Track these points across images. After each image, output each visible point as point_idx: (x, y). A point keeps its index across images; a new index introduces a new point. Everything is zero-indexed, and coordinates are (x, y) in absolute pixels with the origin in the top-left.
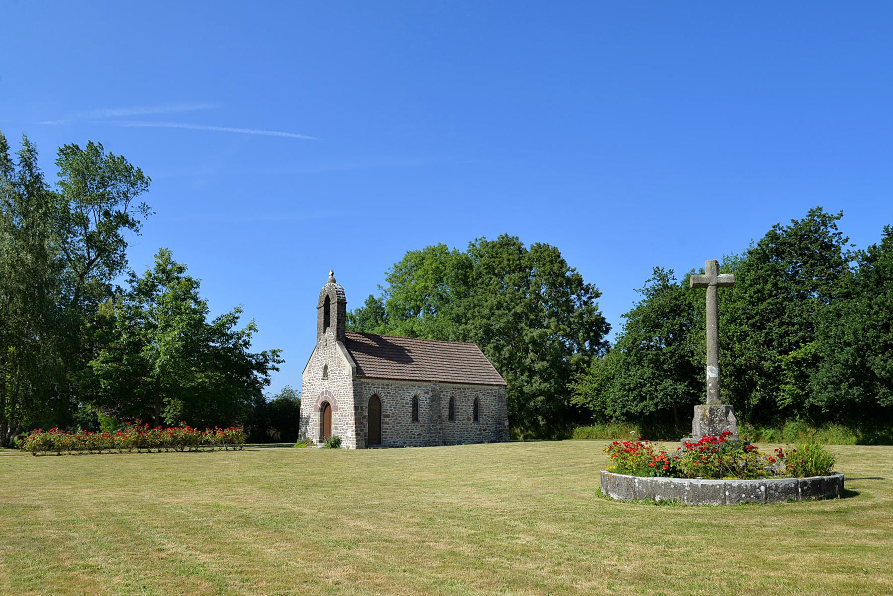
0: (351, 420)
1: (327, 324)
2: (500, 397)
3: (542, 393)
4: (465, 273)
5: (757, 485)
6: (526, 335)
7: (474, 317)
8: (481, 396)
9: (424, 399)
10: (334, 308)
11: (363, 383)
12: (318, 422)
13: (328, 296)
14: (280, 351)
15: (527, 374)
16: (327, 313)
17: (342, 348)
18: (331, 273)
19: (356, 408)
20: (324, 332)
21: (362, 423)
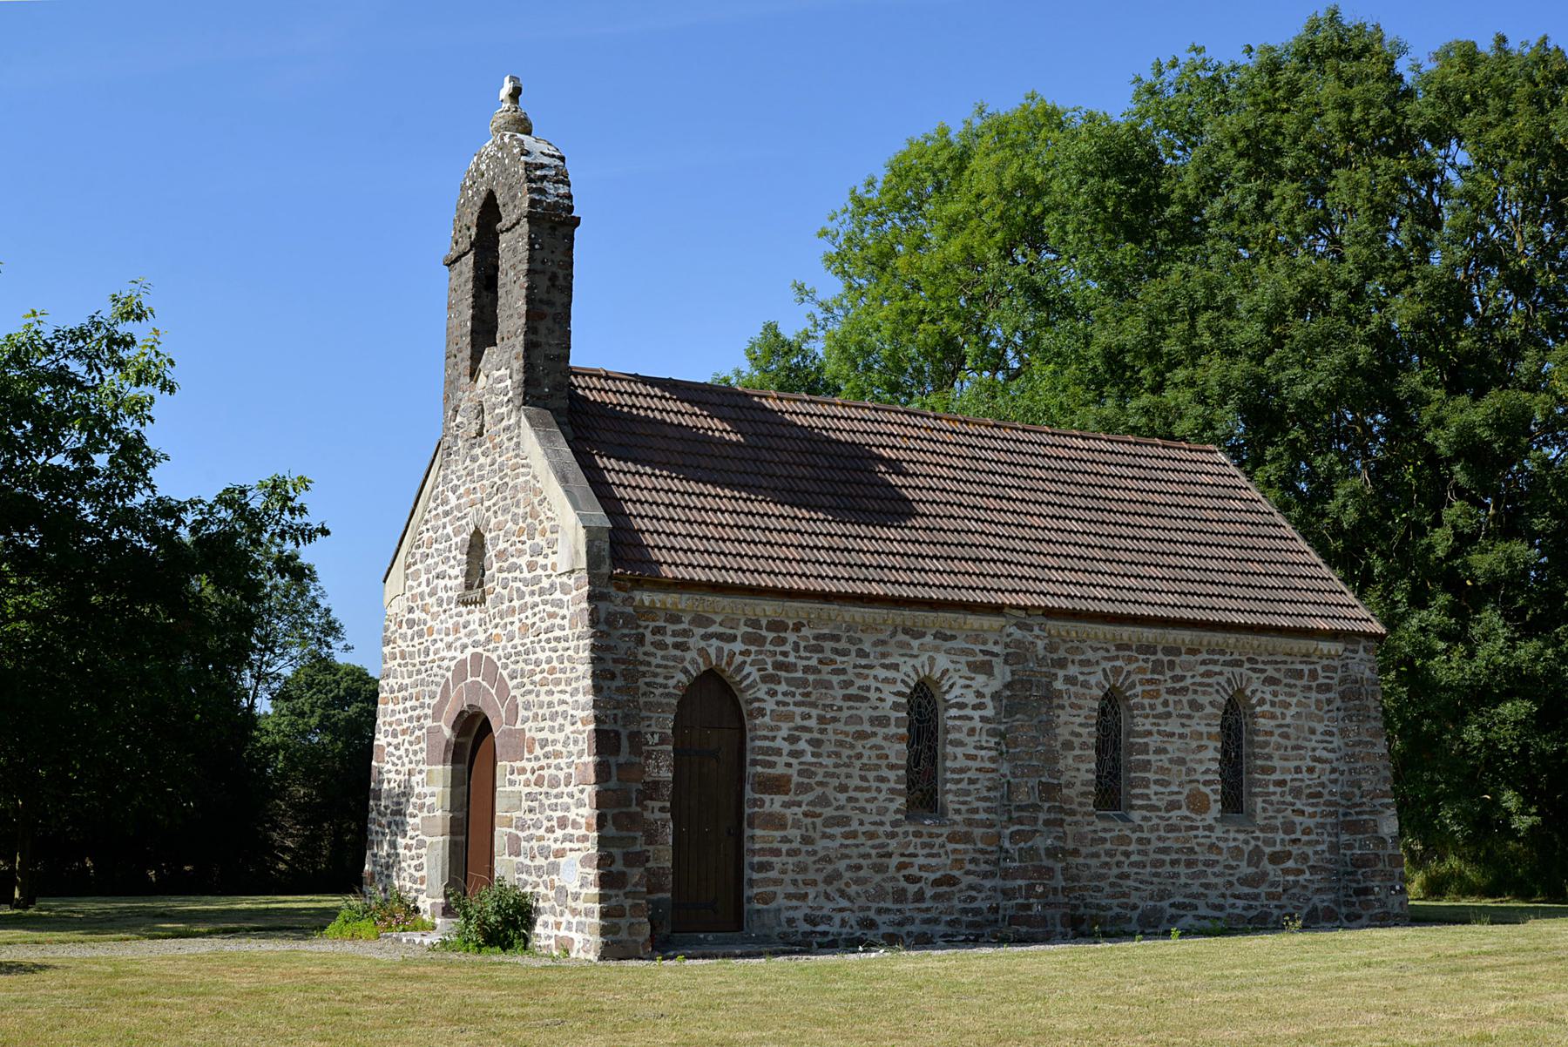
0: (579, 806)
1: (484, 332)
2: (1352, 692)
3: (1517, 683)
4: (1134, 194)
6: (1439, 422)
7: (1195, 353)
8: (1256, 687)
9: (969, 697)
10: (513, 248)
11: (650, 612)
12: (441, 815)
13: (491, 195)
14: (305, 483)
15: (1443, 599)
16: (486, 283)
17: (545, 439)
18: (507, 87)
19: (605, 741)
20: (473, 374)
21: (634, 820)
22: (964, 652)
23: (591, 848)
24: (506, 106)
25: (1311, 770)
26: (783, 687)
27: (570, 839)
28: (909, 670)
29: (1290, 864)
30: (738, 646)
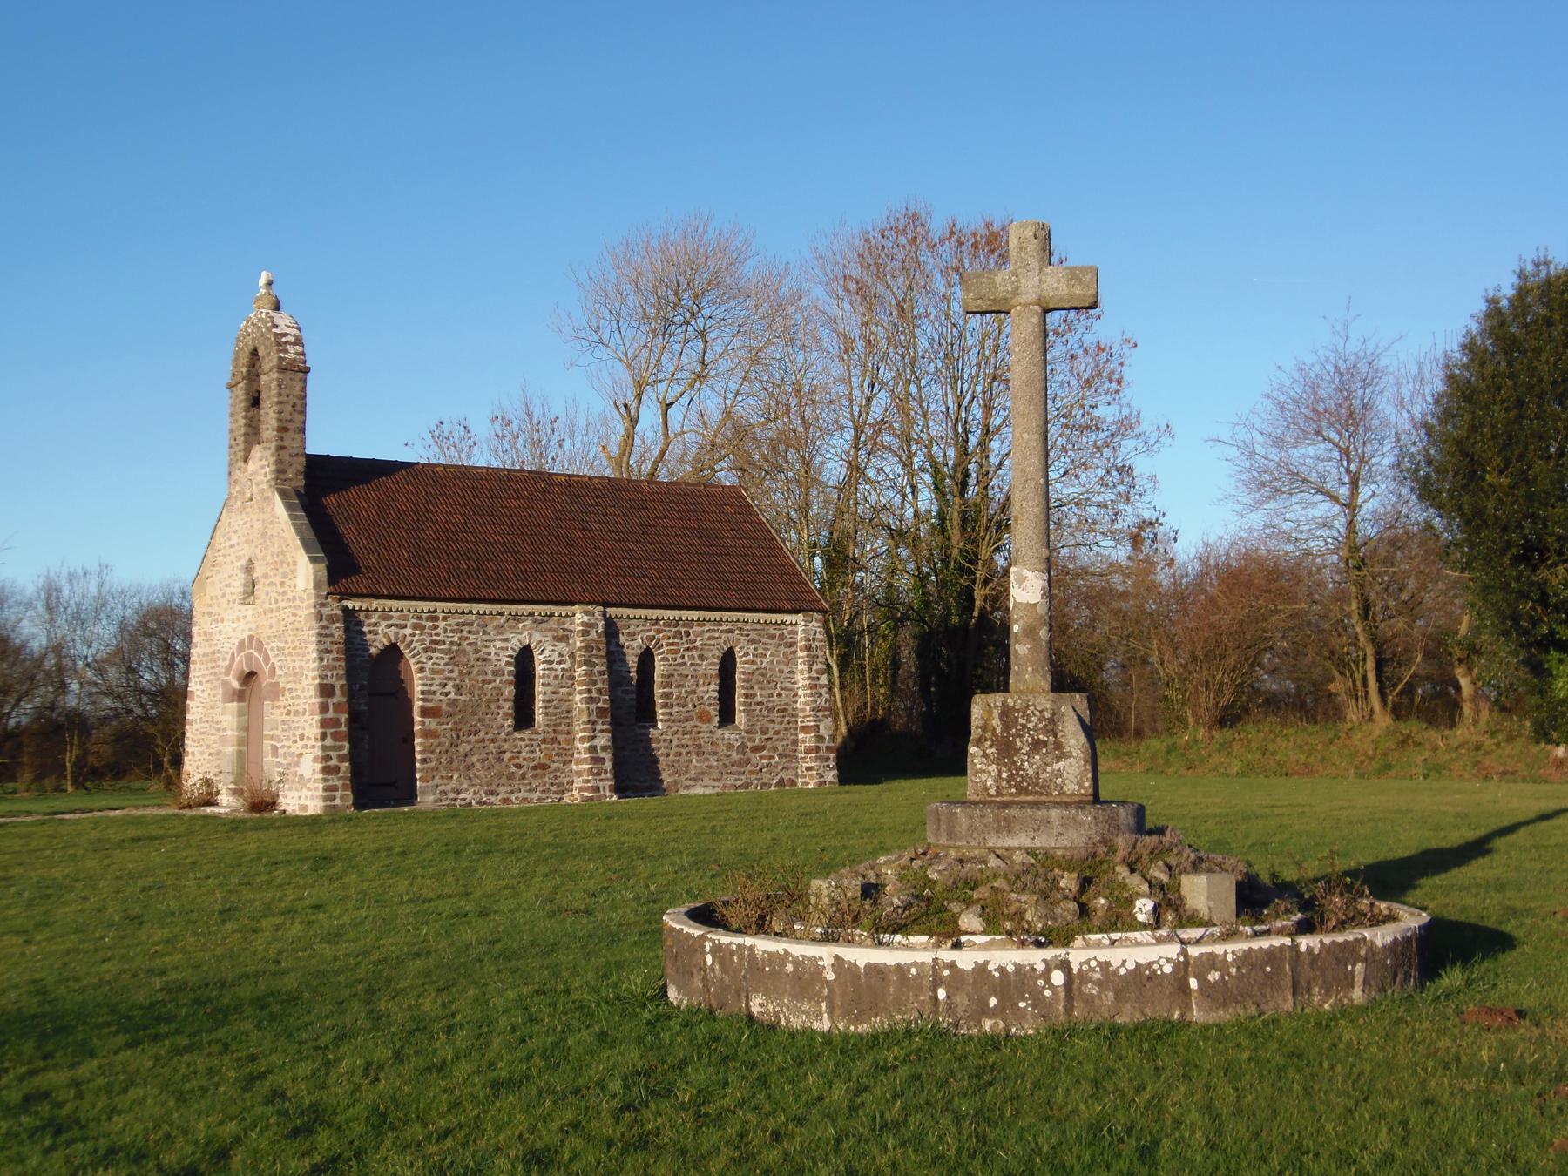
1: (252, 434)
5: (1040, 967)
20: (246, 460)
22: (551, 630)
23: (318, 752)
24: (263, 291)
25: (779, 695)
26: (437, 654)
27: (305, 746)
28: (515, 643)
29: (764, 753)
30: (408, 631)
